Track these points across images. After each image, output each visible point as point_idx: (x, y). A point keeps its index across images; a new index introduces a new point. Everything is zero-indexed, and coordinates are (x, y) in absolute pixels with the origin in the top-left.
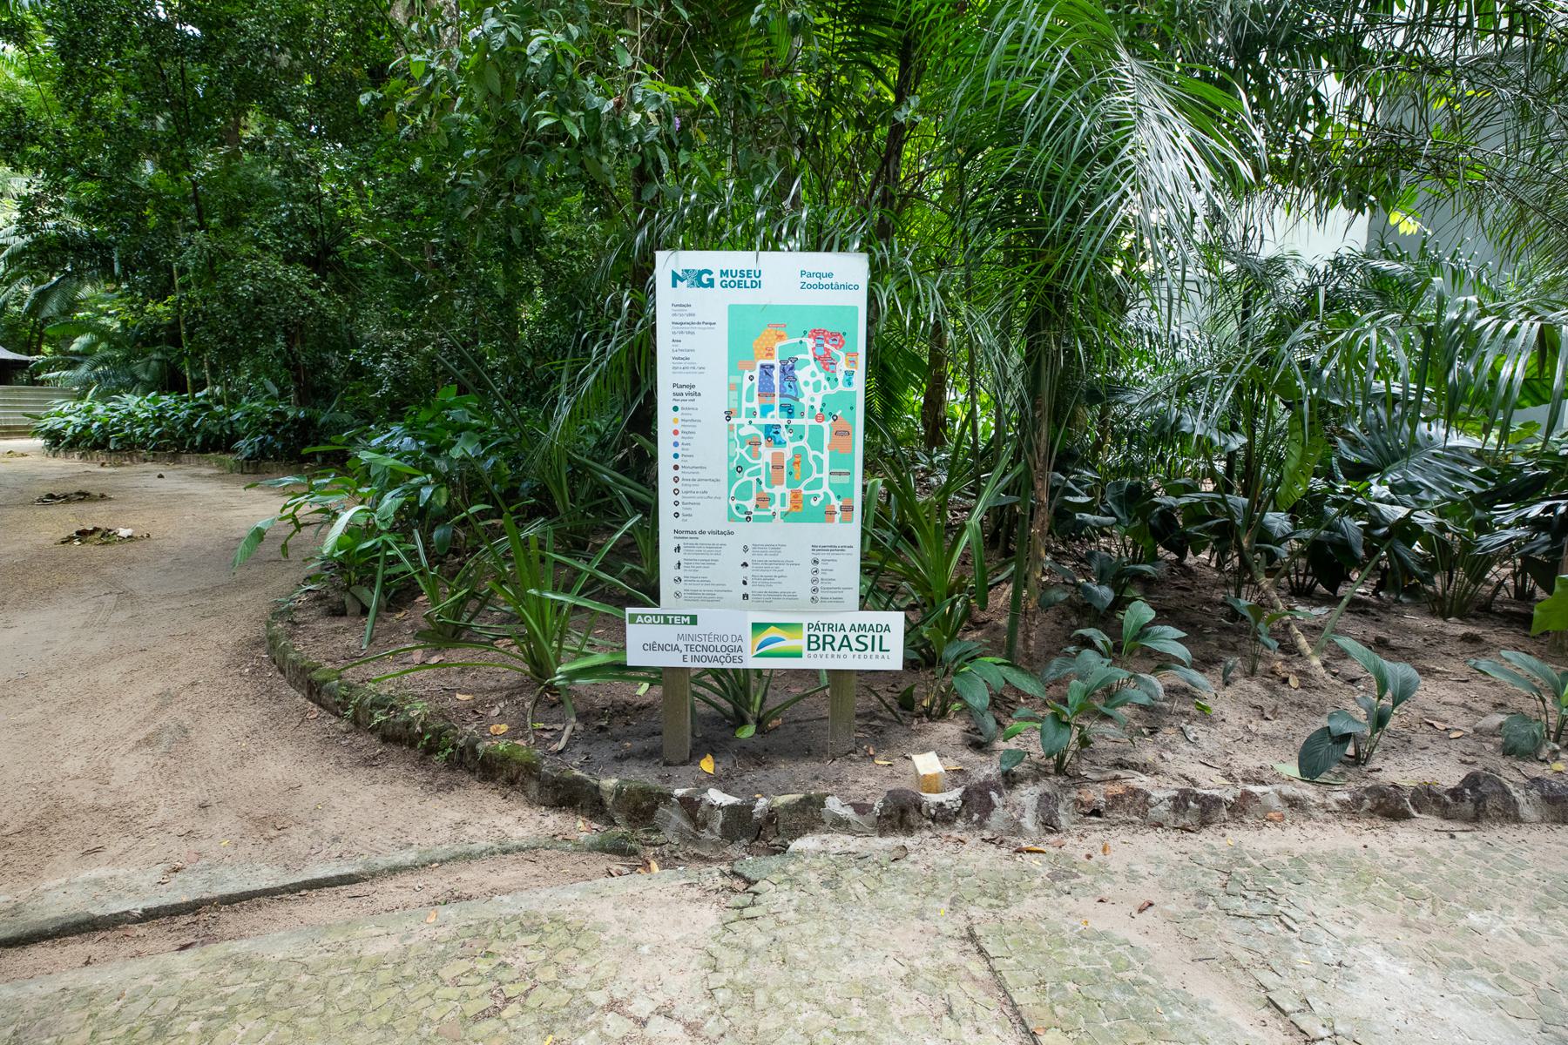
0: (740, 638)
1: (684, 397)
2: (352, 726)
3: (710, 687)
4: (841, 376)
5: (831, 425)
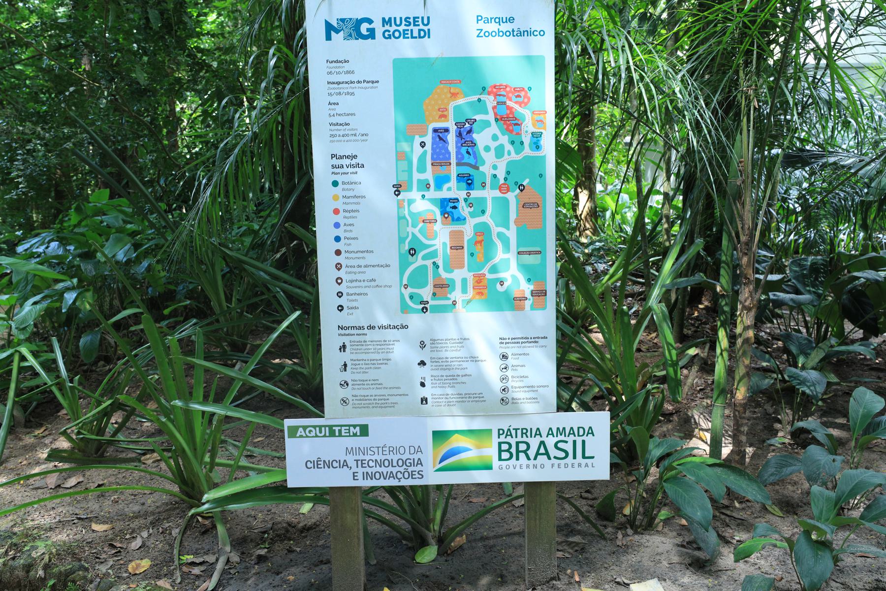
0: (419, 450)
1: (345, 170)
3: (384, 506)
4: (527, 139)
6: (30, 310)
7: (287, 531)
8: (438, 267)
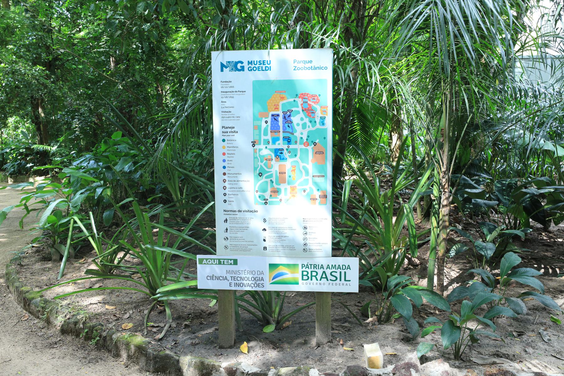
0: (262, 273)
1: (229, 134)
2: (46, 324)
3: (247, 302)
4: (318, 120)
5: (313, 148)
6: (79, 197)
7: (201, 314)
8: (273, 182)
